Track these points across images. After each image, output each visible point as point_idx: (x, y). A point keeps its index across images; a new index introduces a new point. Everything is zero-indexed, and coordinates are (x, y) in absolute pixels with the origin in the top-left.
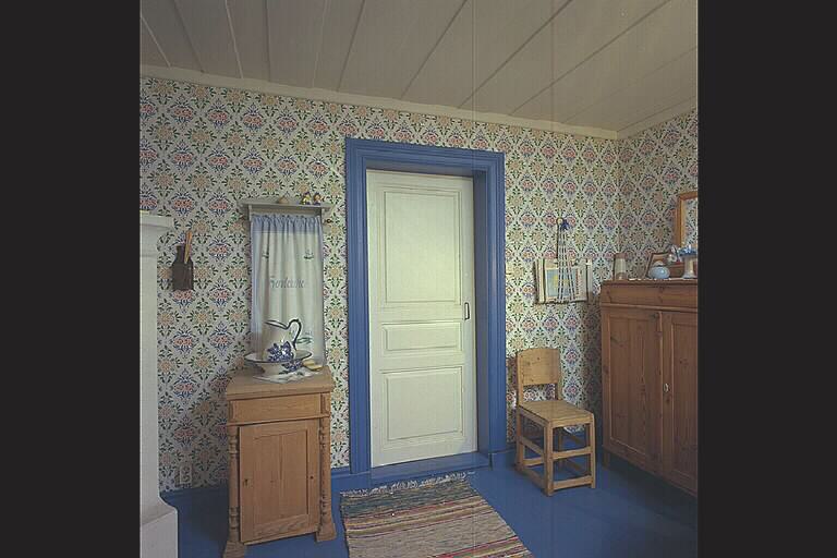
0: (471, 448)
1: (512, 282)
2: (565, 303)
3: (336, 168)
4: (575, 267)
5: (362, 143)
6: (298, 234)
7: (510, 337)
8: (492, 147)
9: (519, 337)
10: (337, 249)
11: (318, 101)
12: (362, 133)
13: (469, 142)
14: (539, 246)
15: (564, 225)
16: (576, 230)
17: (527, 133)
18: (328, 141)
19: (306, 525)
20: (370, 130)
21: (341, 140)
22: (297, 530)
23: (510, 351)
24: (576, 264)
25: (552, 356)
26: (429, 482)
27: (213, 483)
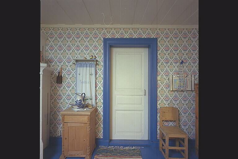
0: (113, 139)
1: (160, 84)
2: (182, 91)
3: (101, 48)
4: (186, 78)
5: (109, 39)
6: (84, 68)
7: (158, 102)
8: (153, 36)
9: (162, 103)
10: (101, 73)
11: (95, 28)
12: (109, 36)
13: (135, 35)
14: (171, 70)
15: (182, 62)
16: (187, 64)
17: (148, 30)
18: (72, 40)
19: (83, 154)
20: (192, 35)
21: (102, 39)
22: (80, 155)
23: (159, 107)
24: (187, 77)
25: (175, 111)
26: (127, 148)
27: (192, 139)
